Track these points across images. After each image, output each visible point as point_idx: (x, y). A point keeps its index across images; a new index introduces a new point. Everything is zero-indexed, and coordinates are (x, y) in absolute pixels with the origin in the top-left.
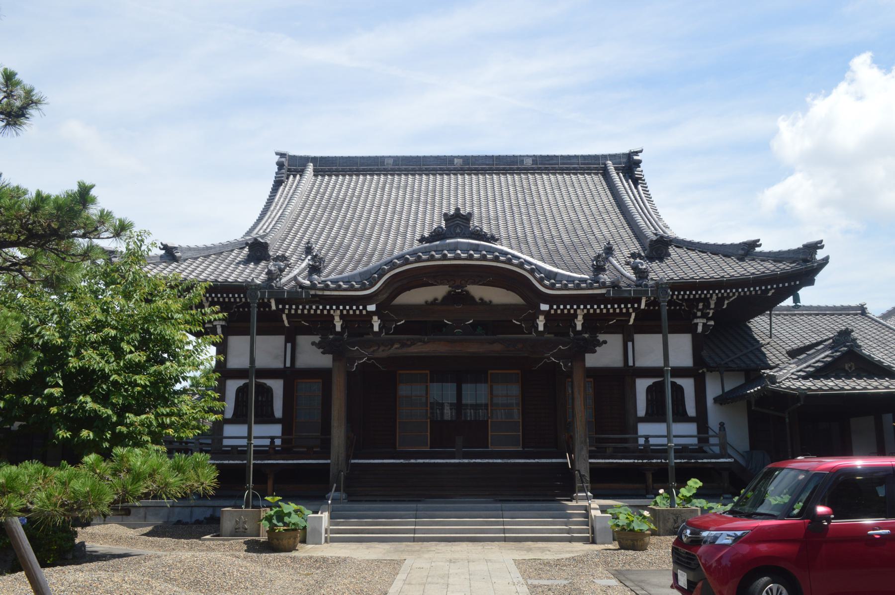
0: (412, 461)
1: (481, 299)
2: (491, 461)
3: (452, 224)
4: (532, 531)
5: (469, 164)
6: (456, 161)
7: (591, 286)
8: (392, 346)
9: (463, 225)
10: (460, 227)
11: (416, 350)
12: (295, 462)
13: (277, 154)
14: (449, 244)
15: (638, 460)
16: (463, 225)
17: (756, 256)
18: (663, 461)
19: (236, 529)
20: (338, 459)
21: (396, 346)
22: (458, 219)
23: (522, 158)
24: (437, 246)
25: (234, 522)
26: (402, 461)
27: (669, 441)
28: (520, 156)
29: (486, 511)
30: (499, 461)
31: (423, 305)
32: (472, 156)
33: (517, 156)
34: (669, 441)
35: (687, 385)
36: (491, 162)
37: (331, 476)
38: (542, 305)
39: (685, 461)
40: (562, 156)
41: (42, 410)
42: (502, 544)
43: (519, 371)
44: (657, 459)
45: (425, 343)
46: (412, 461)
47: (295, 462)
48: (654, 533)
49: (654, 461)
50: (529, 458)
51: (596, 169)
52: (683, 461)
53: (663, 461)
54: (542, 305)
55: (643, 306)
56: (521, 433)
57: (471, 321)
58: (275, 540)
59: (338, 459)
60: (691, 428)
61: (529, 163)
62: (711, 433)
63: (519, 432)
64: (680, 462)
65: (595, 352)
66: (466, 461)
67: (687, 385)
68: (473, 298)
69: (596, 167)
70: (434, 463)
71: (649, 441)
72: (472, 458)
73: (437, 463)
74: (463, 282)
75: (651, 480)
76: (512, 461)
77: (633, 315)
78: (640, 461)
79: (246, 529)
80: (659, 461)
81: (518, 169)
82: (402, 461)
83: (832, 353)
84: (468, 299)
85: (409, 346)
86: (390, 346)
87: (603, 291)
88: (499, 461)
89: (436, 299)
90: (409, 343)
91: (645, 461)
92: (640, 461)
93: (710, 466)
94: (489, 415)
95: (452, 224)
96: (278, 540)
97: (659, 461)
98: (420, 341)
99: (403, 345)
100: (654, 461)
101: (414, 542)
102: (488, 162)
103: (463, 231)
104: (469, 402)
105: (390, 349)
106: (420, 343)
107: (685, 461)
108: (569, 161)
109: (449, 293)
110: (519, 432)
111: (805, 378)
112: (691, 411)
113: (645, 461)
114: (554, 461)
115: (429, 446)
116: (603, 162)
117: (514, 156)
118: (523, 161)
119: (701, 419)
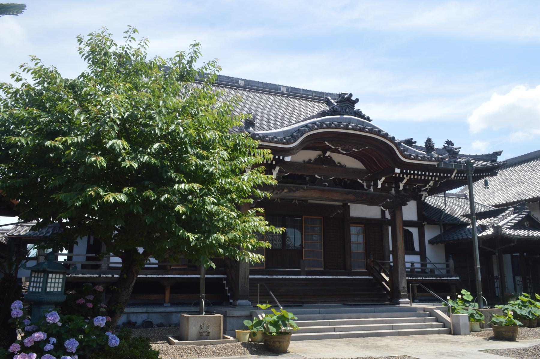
0: (275, 277)
1: (339, 163)
2: (326, 277)
3: (344, 105)
4: (409, 327)
5: (248, 85)
6: (240, 82)
7: (424, 159)
8: (283, 190)
9: (351, 107)
10: (349, 108)
11: (298, 195)
12: (189, 276)
13: (11, 76)
14: (346, 118)
15: (411, 277)
16: (351, 107)
17: (460, 156)
18: (424, 278)
19: (200, 333)
20: (245, 274)
21: (286, 190)
22: (348, 102)
23: (280, 87)
24: (337, 118)
25: (198, 327)
26: (267, 277)
27: (32, 287)
28: (279, 85)
29: (303, 314)
30: (331, 277)
31: (302, 163)
32: (250, 80)
33: (277, 85)
34: (32, 287)
35: (414, 231)
36: (262, 86)
37: (240, 287)
38: (396, 169)
39: (435, 278)
40: (303, 89)
41: (169, 206)
42: (398, 337)
43: (322, 218)
44: (421, 277)
45: (305, 190)
46: (275, 277)
47: (189, 276)
48: (520, 326)
49: (419, 278)
50: (349, 275)
51: (322, 100)
52: (434, 278)
53: (424, 278)
54: (396, 169)
55: (453, 176)
56: (323, 259)
57: (333, 178)
58: (277, 343)
59: (245, 274)
60: (416, 258)
61: (284, 90)
62: (428, 261)
63: (322, 258)
64: (433, 279)
65: (407, 205)
66: (310, 277)
67: (414, 231)
68: (334, 162)
69: (322, 99)
70: (297, 278)
71: (414, 266)
72: (314, 275)
73: (291, 278)
74: (350, 147)
75: (416, 291)
76: (339, 277)
77: (418, 184)
78: (412, 278)
79: (209, 333)
80: (421, 278)
81: (278, 93)
82: (267, 277)
83: (518, 215)
84: (330, 161)
85: (294, 191)
86: (281, 191)
87: (435, 163)
88: (331, 277)
89: (310, 160)
90: (294, 189)
91: (414, 278)
92: (412, 278)
93: (446, 282)
94: (304, 246)
95: (344, 105)
96: (280, 342)
97: (421, 278)
98: (302, 188)
99: (290, 190)
100: (419, 278)
101: (340, 338)
102: (259, 86)
103: (351, 112)
104: (354, 233)
105: (281, 192)
106: (301, 190)
107: (435, 278)
108: (307, 93)
109: (319, 156)
110: (322, 258)
111: (510, 229)
112: (417, 248)
113: (414, 278)
114: (364, 277)
115: (265, 267)
116: (326, 97)
117: (271, 84)
118: (281, 88)
119: (422, 253)
